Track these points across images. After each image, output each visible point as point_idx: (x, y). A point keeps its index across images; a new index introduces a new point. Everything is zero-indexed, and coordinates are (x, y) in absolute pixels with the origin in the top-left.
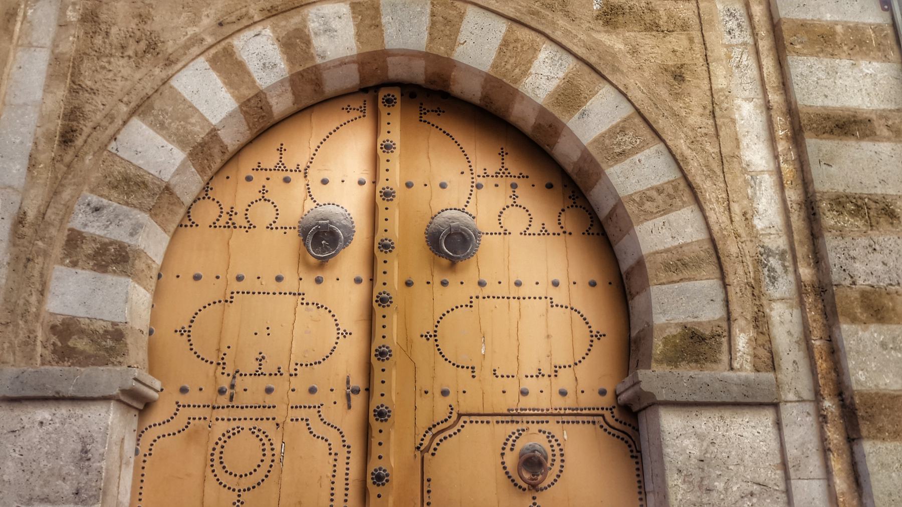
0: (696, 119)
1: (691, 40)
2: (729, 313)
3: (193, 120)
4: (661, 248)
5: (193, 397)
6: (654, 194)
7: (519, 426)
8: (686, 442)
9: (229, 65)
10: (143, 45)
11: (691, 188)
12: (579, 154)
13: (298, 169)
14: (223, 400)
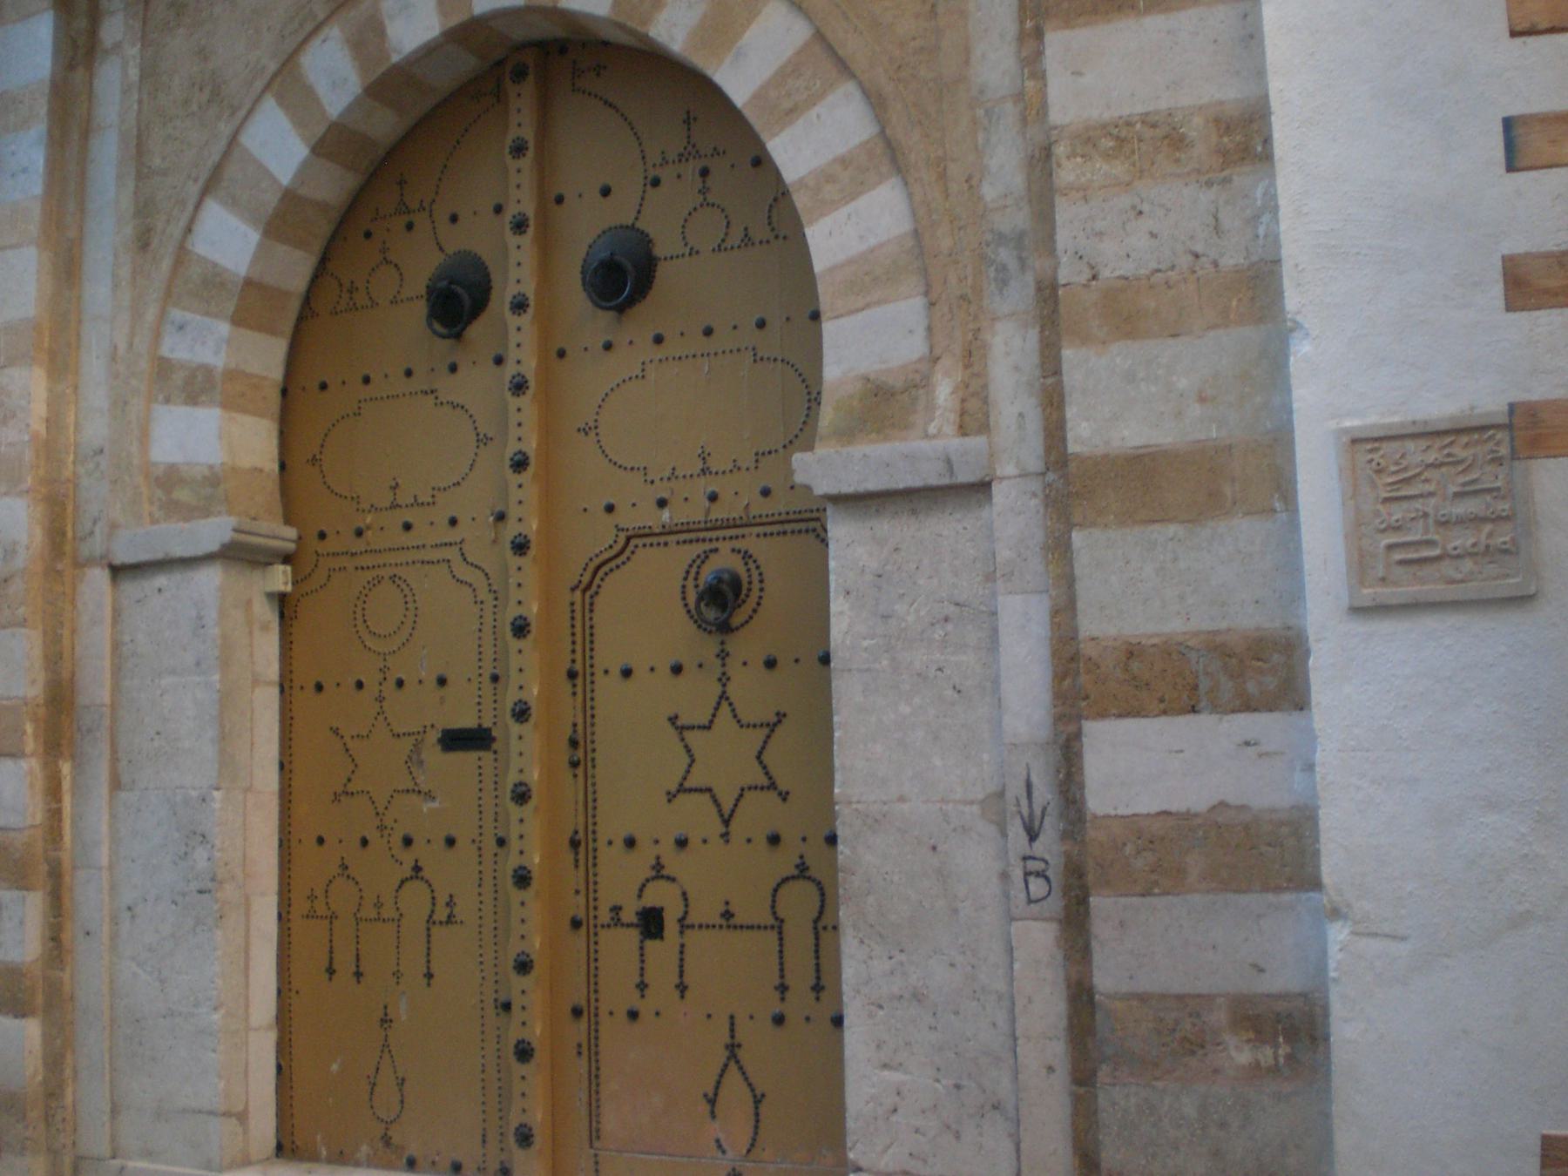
7: (707, 546)
10: (206, 95)
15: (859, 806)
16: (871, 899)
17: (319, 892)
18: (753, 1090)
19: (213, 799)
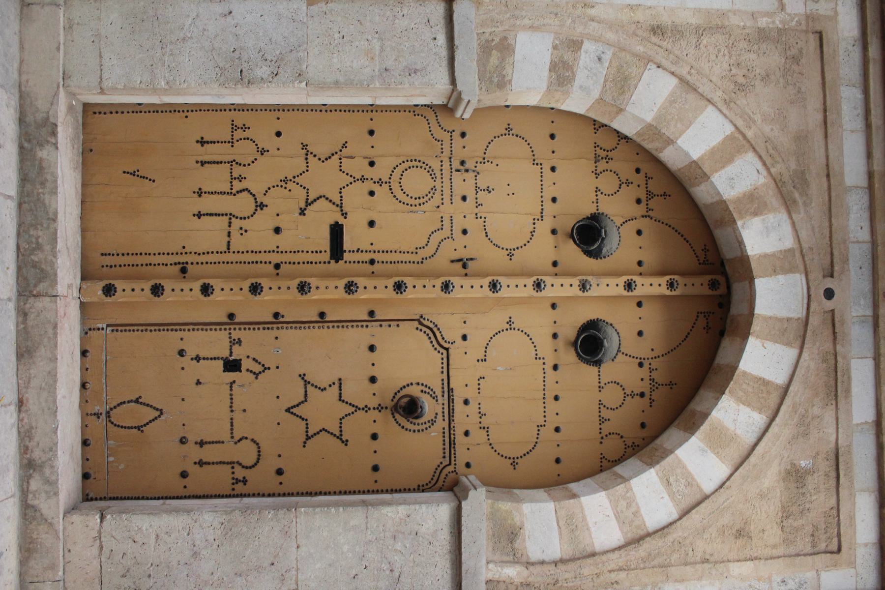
0: (701, 547)
1: (774, 547)
2: (533, 564)
3: (679, 125)
4: (587, 512)
5: (458, 141)
6: (633, 509)
8: (430, 523)
9: (725, 153)
10: (741, 80)
11: (639, 540)
12: (669, 448)
13: (648, 210)
14: (456, 164)
15: (294, 523)
16: (245, 529)
17: (247, 134)
18: (145, 425)
19: (300, 82)
